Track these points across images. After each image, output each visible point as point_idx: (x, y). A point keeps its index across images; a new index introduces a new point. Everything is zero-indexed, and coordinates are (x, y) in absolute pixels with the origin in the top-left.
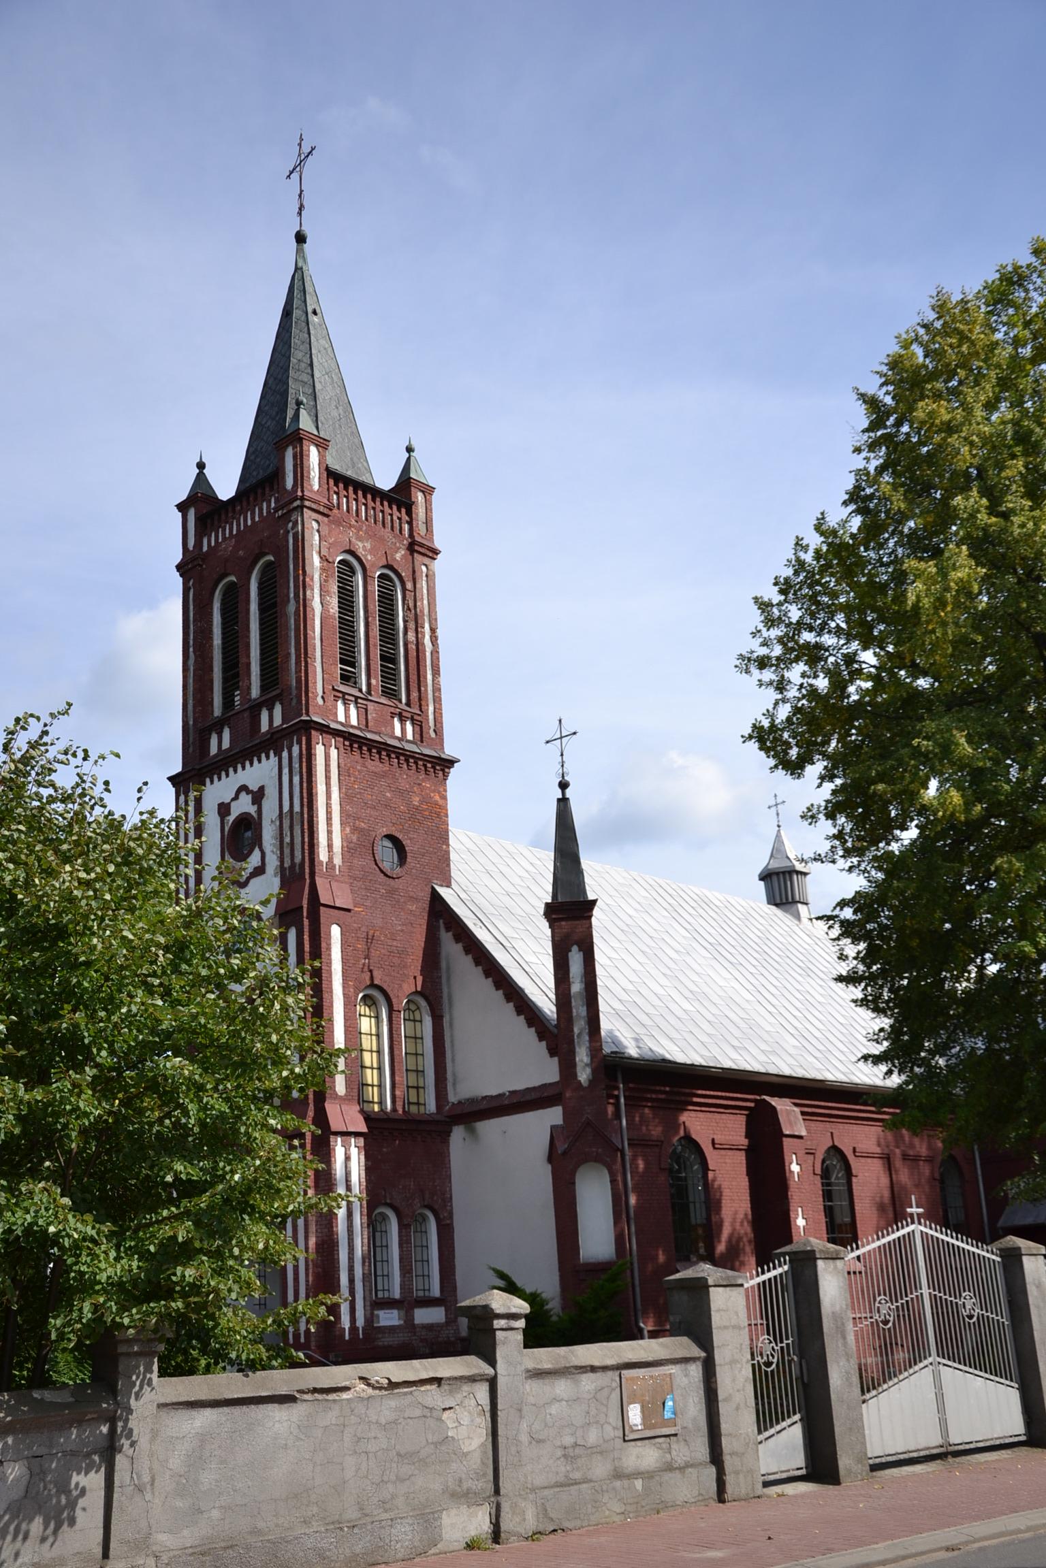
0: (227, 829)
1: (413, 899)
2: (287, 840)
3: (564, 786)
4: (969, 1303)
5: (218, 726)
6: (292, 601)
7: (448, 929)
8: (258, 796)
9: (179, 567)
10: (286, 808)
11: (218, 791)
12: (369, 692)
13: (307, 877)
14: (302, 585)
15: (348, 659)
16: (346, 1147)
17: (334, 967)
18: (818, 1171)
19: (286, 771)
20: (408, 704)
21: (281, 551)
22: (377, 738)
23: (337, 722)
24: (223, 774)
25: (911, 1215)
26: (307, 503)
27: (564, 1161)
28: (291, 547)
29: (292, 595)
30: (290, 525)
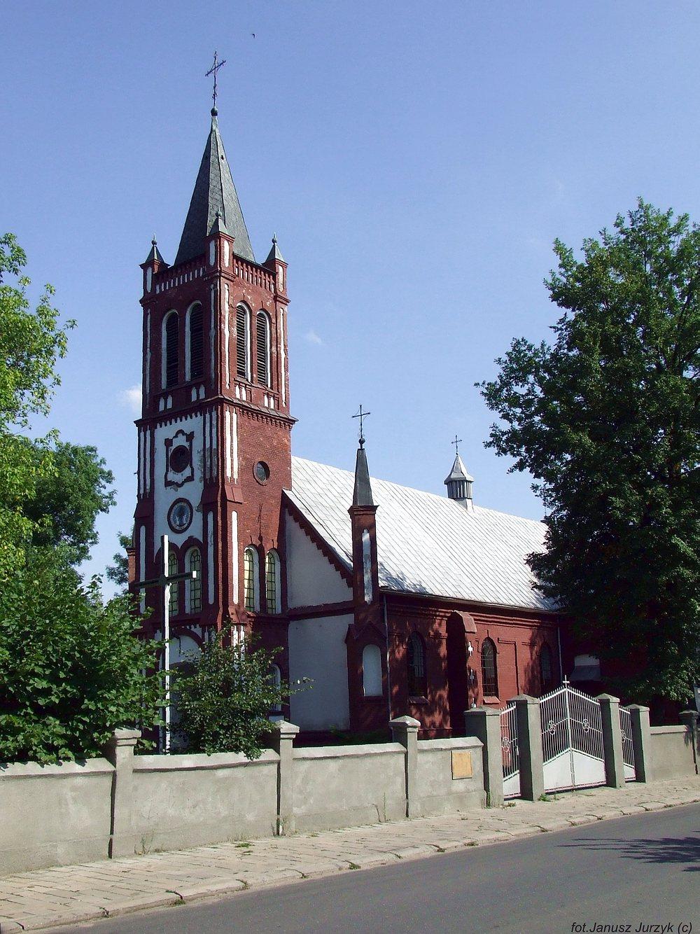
0: (170, 454)
1: (275, 498)
2: (208, 463)
3: (362, 442)
4: (585, 723)
5: (165, 396)
6: (213, 330)
7: (290, 514)
8: (190, 437)
9: (141, 301)
10: (208, 446)
11: (164, 432)
12: (252, 382)
13: (220, 484)
14: (219, 321)
15: (241, 360)
16: (239, 630)
17: (209, 527)
18: (480, 650)
19: (208, 425)
20: (272, 388)
21: (206, 300)
22: (257, 408)
23: (236, 398)
24: (168, 422)
25: (564, 684)
26: (223, 274)
27: (355, 644)
28: (213, 298)
29: (213, 326)
30: (212, 286)
